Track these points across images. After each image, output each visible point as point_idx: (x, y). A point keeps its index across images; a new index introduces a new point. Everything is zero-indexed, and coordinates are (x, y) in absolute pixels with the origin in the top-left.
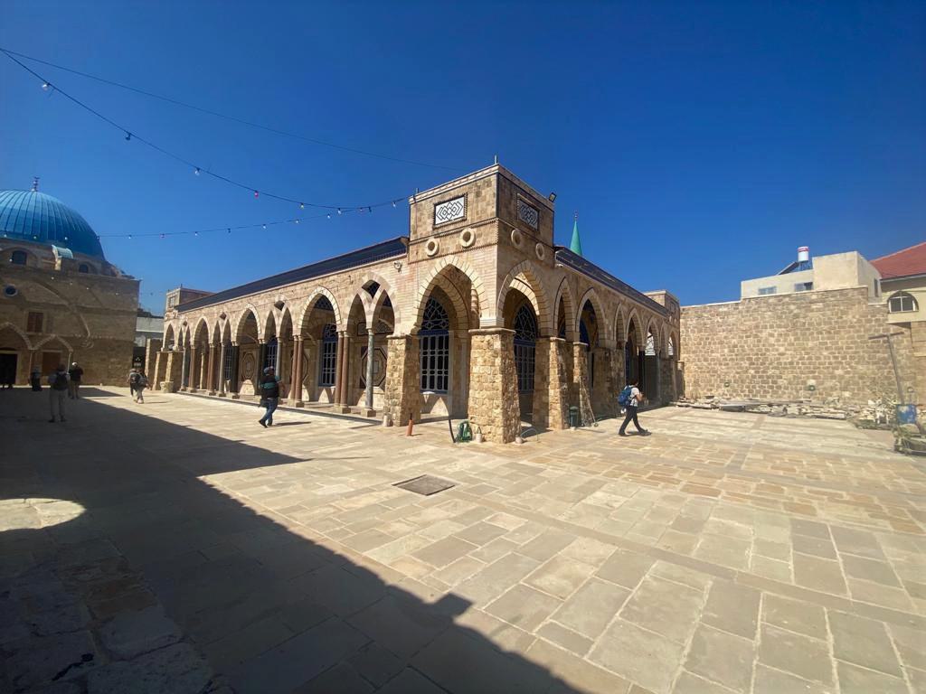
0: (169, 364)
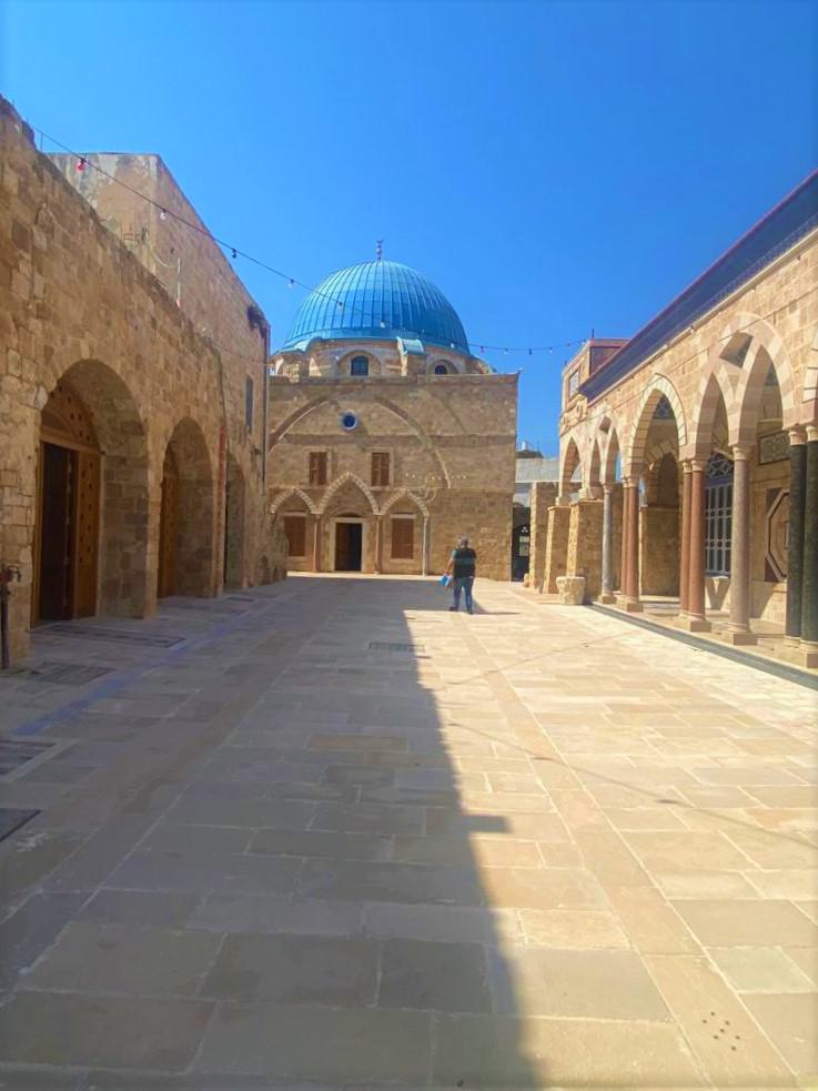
0: (573, 532)
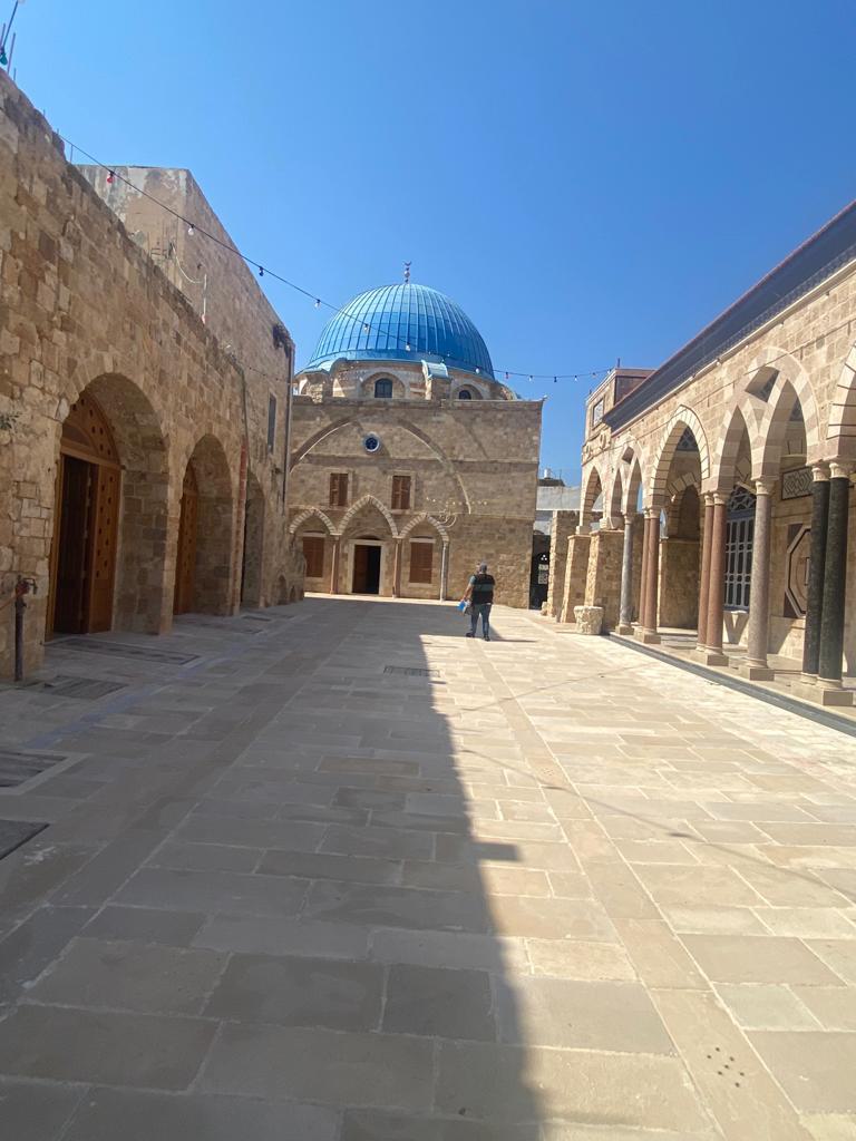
0: (593, 561)
